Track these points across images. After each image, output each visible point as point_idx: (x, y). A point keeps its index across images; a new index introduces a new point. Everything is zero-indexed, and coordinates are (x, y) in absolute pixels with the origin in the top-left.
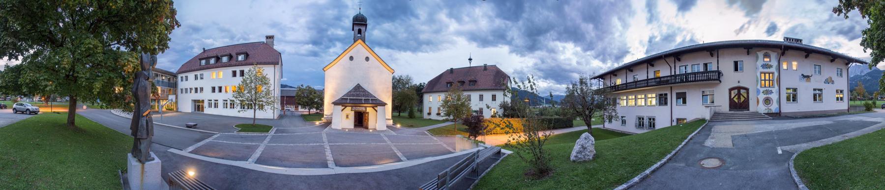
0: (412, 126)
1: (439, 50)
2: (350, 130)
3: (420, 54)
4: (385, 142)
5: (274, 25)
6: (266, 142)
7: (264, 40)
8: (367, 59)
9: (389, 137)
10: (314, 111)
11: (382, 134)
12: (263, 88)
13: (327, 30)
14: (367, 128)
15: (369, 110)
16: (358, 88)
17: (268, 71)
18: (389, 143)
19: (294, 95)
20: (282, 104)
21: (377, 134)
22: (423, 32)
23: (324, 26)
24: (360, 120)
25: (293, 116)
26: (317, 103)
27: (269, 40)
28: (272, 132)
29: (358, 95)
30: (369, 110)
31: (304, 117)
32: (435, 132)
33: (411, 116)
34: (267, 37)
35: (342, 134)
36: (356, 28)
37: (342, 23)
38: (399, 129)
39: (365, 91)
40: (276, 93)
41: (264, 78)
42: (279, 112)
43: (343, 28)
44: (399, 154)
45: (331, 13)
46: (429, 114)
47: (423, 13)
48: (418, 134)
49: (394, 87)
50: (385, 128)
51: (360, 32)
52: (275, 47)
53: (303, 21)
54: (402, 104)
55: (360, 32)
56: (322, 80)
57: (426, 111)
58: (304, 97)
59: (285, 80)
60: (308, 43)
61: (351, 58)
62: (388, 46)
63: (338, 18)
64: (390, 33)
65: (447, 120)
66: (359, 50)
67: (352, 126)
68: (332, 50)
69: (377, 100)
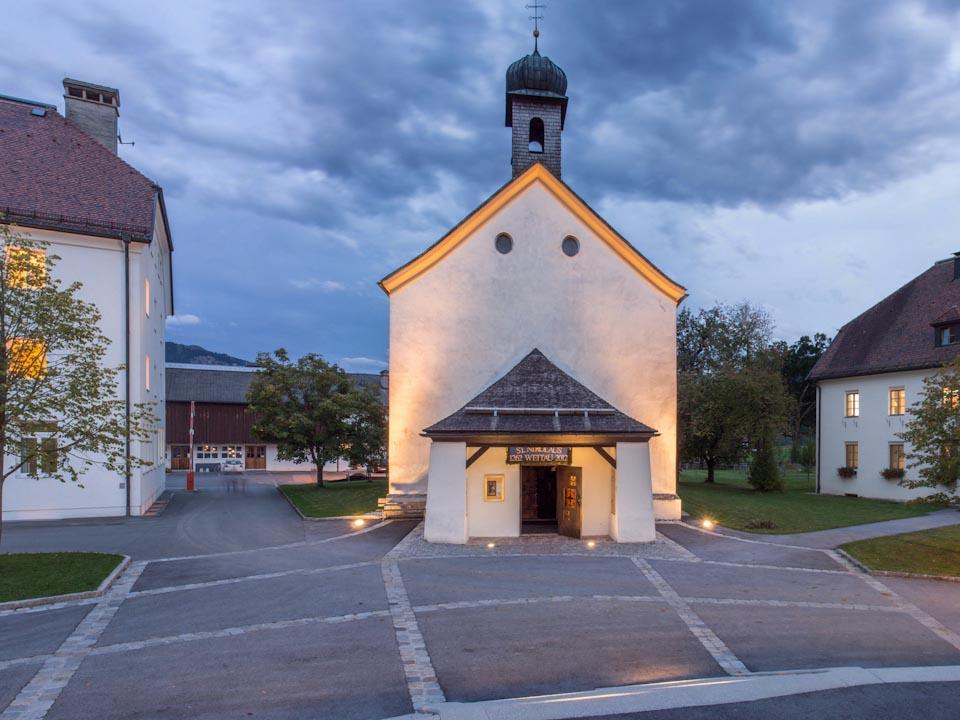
0: (766, 527)
1: (893, 175)
2: (515, 539)
3: (801, 209)
4: (649, 589)
5: (117, 38)
6: (80, 641)
7: (57, 99)
8: (571, 245)
9: (669, 570)
10: (339, 468)
11: (637, 560)
12: (55, 358)
13: (392, 114)
14: (574, 533)
15: (582, 457)
16: (535, 366)
17: (87, 270)
18: (668, 594)
19: (242, 394)
20: (177, 440)
21: (616, 554)
22: (816, 106)
23: (379, 95)
24: (546, 501)
25: (235, 493)
26: (352, 433)
27: (82, 106)
28: (120, 585)
29: (533, 399)
30: (582, 457)
31: (292, 498)
32: (877, 557)
33: (764, 482)
34: (74, 89)
35: (470, 561)
36: (523, 116)
37: (463, 93)
38: (707, 539)
39: (563, 379)
40: (144, 383)
41: (63, 301)
42: (161, 482)
43: (466, 114)
44: (713, 645)
45: (411, 41)
46: (847, 473)
47: (812, 30)
48: (796, 560)
49: (686, 361)
50: (650, 534)
51: (537, 131)
52: (123, 151)
53: (278, 54)
54: (720, 430)
55: (537, 131)
56: (378, 334)
57: (831, 457)
58: (288, 409)
59: (186, 323)
60: (304, 163)
61: (504, 242)
62: (657, 185)
63: (445, 68)
64: (665, 131)
65: (937, 504)
66: (537, 208)
67: (512, 530)
68: (418, 204)
69: (614, 415)
